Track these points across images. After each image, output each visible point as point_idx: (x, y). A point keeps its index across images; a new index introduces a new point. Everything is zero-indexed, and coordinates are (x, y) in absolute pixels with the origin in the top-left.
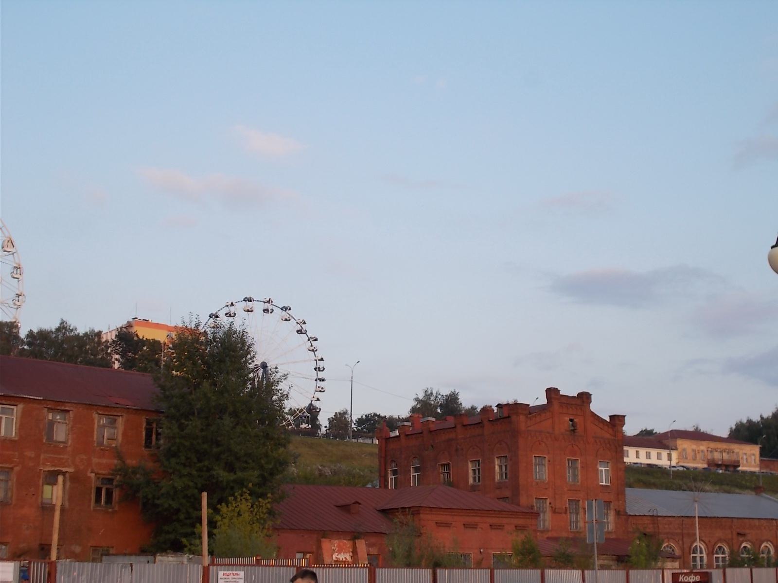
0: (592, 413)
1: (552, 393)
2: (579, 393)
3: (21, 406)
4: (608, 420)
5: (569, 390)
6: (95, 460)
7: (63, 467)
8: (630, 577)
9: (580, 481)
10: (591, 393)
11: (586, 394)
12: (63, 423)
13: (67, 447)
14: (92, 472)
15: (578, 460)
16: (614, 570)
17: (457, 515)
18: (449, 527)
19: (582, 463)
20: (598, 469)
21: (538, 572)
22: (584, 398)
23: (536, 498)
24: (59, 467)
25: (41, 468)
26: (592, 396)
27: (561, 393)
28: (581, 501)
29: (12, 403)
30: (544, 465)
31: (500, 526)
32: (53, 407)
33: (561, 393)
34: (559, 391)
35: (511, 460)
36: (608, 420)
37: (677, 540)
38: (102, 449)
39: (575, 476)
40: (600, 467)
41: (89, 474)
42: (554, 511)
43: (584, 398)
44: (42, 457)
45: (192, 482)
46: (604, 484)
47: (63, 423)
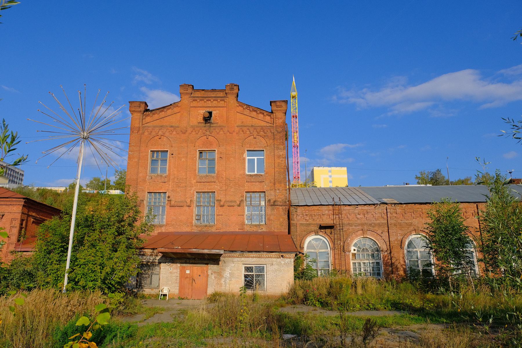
37: (379, 232)
46: (256, 173)
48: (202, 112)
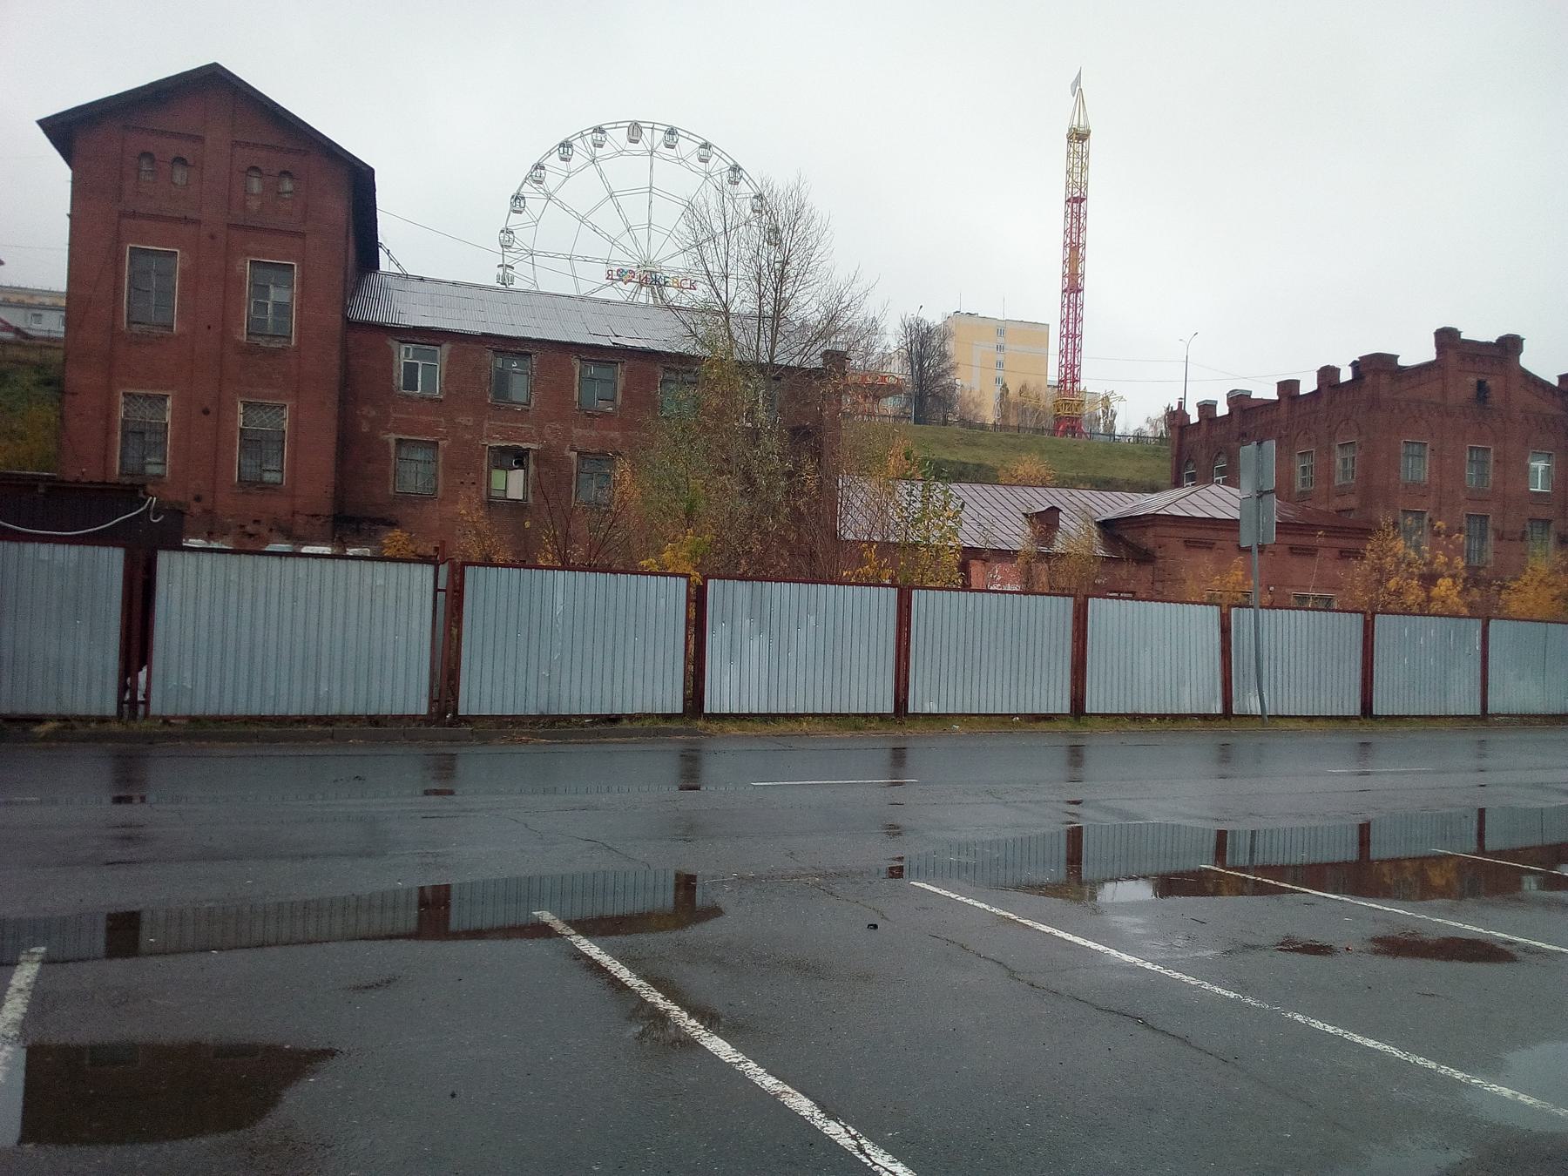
0: (1524, 370)
1: (1447, 338)
2: (1437, 330)
3: (446, 347)
4: (1555, 382)
5: (1480, 329)
6: (577, 432)
7: (523, 442)
8: (432, 581)
9: (1491, 484)
10: (1522, 336)
11: (1512, 338)
12: (521, 373)
13: (528, 410)
14: (572, 450)
15: (1490, 449)
16: (1143, 600)
17: (1225, 530)
18: (1211, 548)
19: (1497, 454)
20: (1528, 466)
21: (111, 561)
22: (1510, 345)
23: (1404, 511)
24: (516, 441)
25: (486, 443)
26: (1524, 341)
27: (1463, 336)
28: (1491, 517)
29: (432, 341)
30: (1424, 457)
31: (1307, 549)
32: (503, 348)
33: (1463, 336)
34: (1460, 333)
35: (1361, 448)
36: (1555, 382)
38: (589, 415)
39: (1482, 475)
40: (1532, 461)
41: (567, 453)
42: (1500, 537)
43: (1510, 345)
44: (486, 425)
45: (1440, 509)
46: (1539, 490)
47: (521, 373)
48: (1473, 380)
